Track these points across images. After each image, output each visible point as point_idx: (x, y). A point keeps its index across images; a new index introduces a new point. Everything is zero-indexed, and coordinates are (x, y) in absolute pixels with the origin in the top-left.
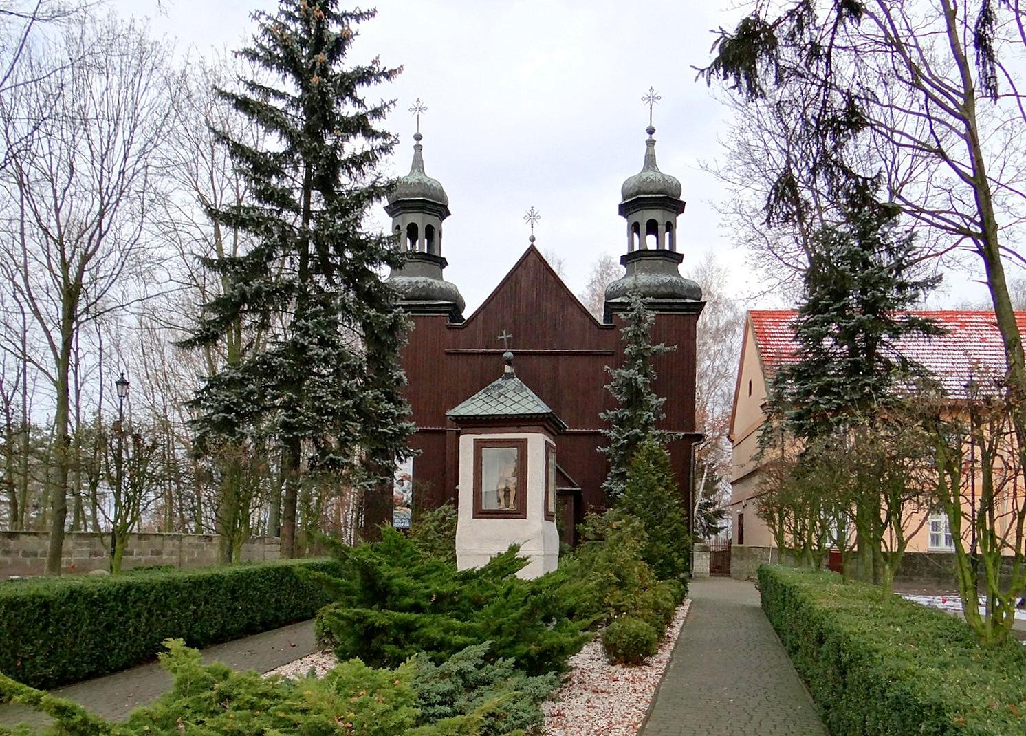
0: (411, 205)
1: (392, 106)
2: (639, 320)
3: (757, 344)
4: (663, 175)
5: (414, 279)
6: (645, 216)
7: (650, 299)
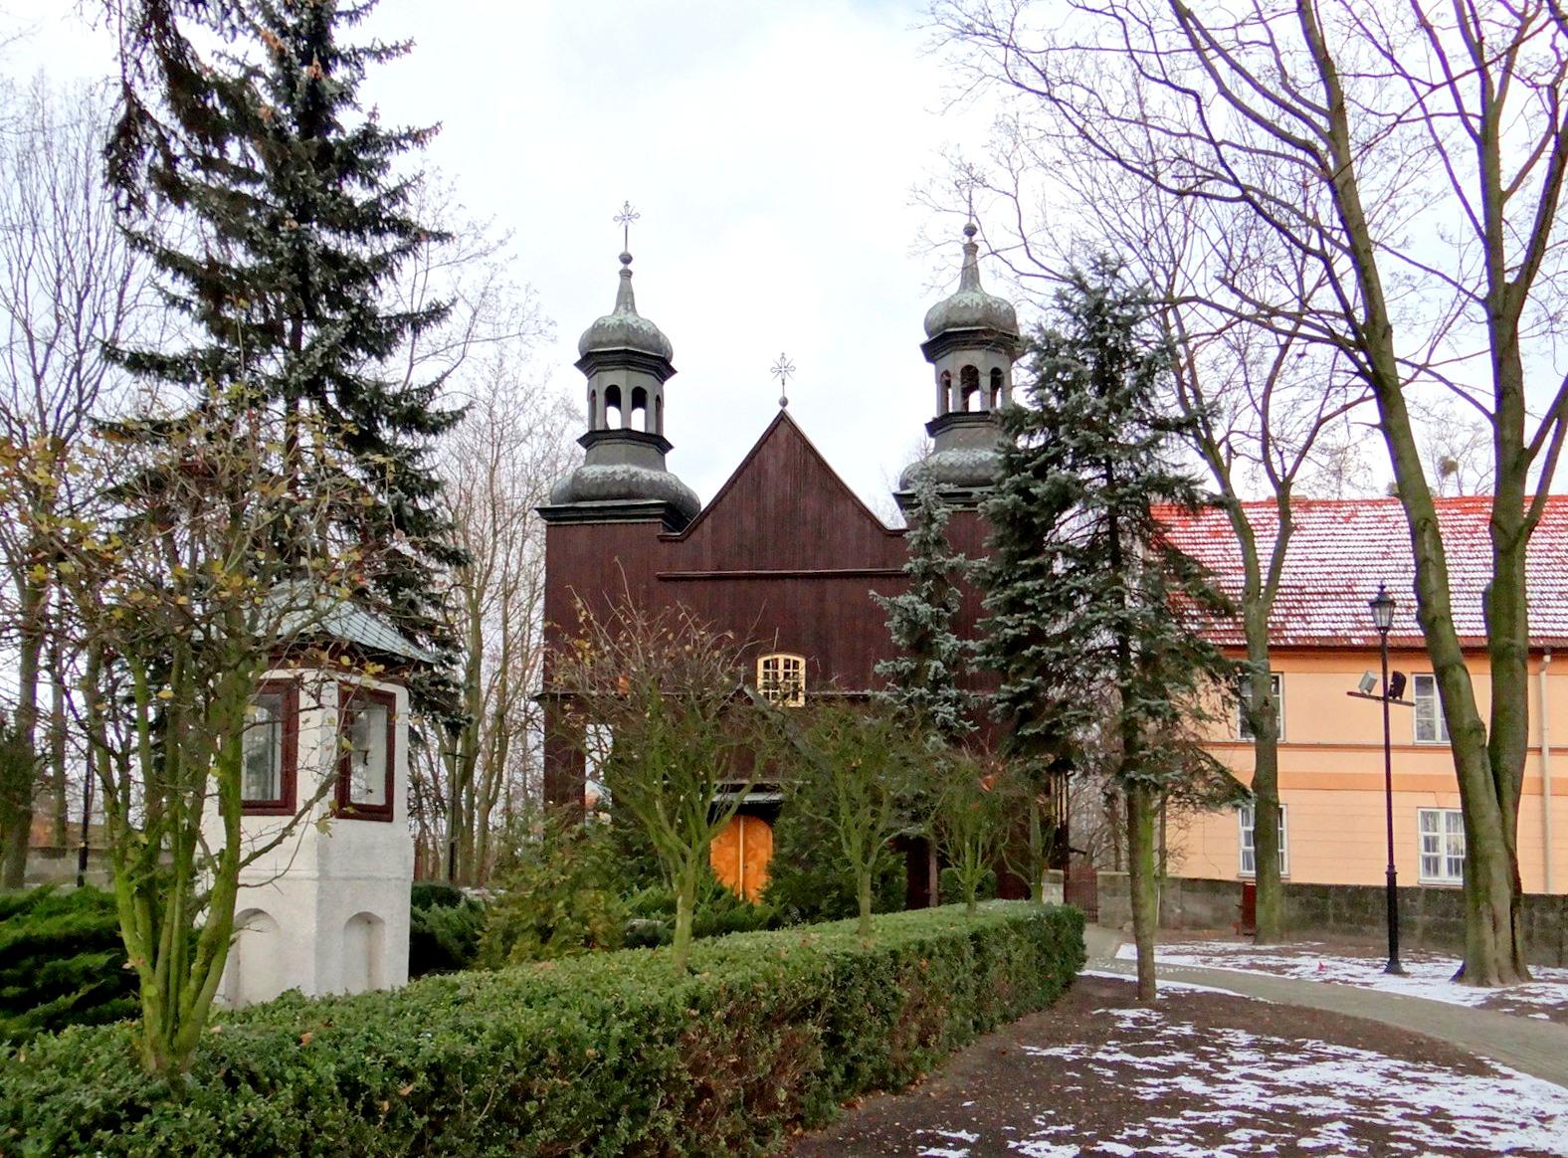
0: (611, 358)
1: (415, 183)
5: (609, 469)
6: (957, 361)
7: (946, 488)
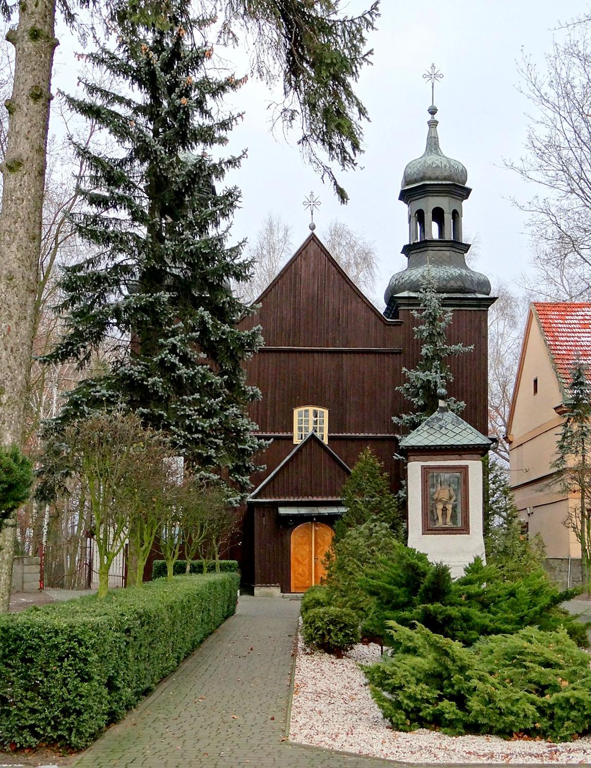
1: (239, 119)
2: (433, 320)
3: (545, 341)
4: (448, 160)
